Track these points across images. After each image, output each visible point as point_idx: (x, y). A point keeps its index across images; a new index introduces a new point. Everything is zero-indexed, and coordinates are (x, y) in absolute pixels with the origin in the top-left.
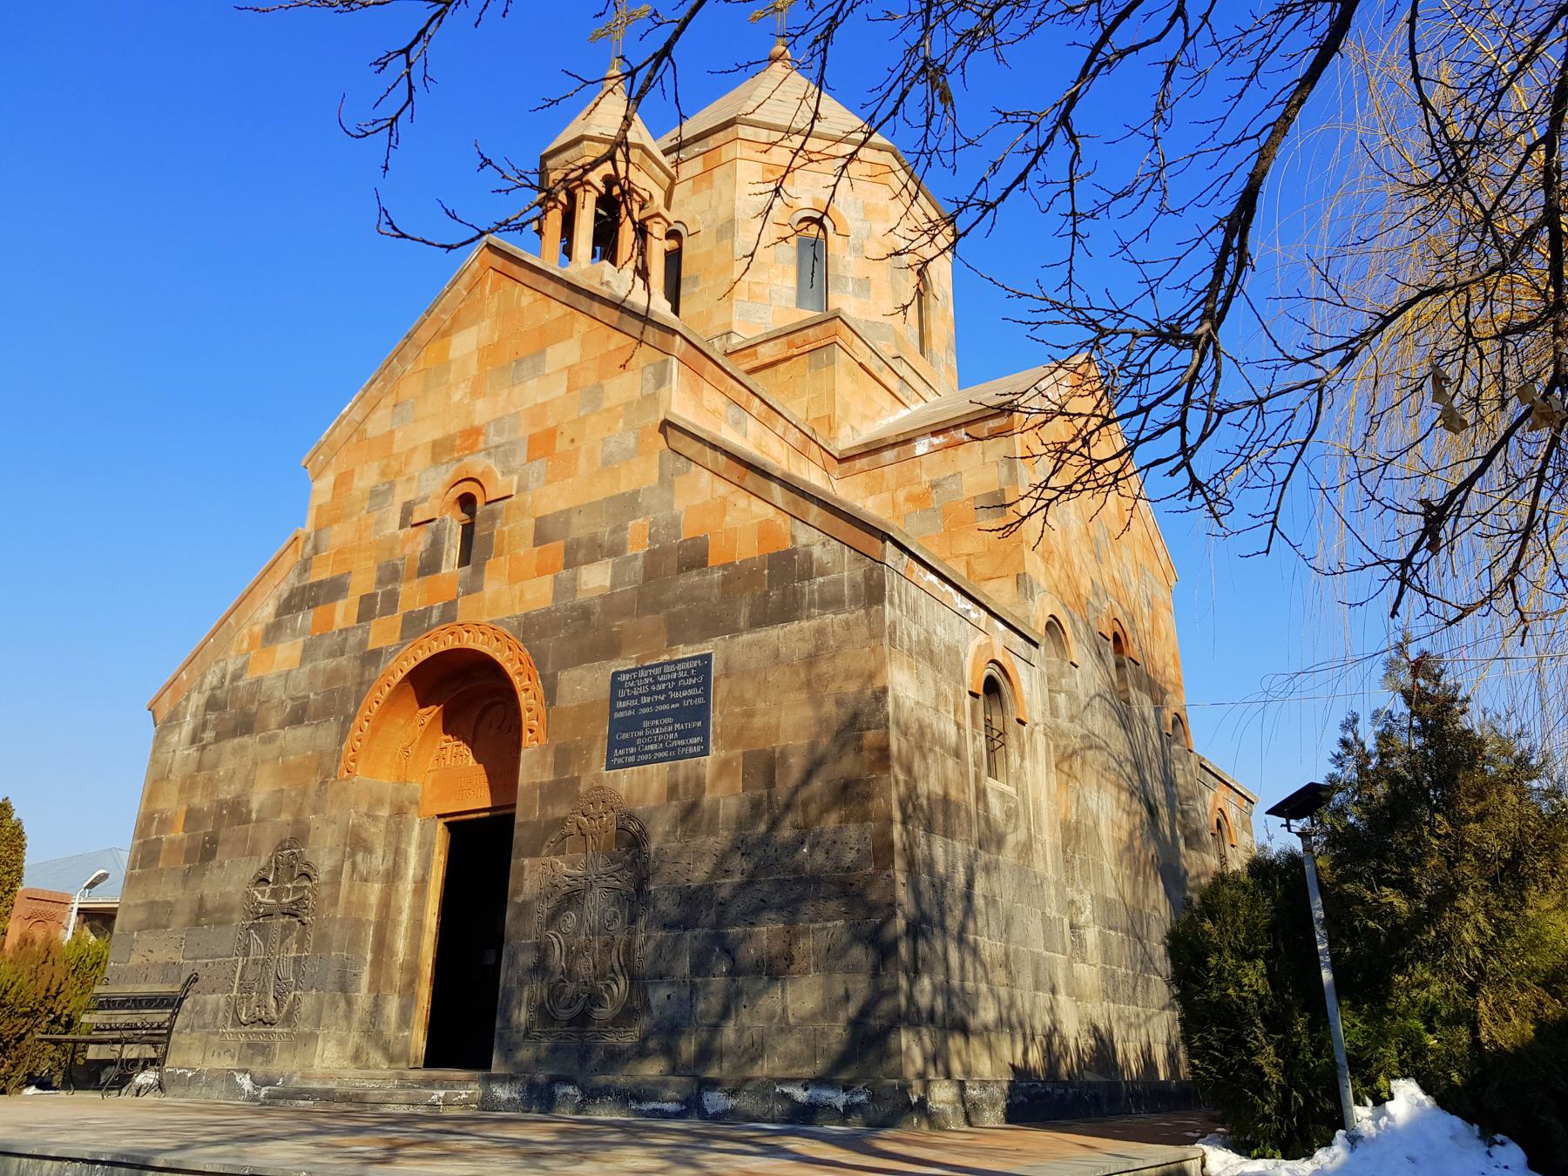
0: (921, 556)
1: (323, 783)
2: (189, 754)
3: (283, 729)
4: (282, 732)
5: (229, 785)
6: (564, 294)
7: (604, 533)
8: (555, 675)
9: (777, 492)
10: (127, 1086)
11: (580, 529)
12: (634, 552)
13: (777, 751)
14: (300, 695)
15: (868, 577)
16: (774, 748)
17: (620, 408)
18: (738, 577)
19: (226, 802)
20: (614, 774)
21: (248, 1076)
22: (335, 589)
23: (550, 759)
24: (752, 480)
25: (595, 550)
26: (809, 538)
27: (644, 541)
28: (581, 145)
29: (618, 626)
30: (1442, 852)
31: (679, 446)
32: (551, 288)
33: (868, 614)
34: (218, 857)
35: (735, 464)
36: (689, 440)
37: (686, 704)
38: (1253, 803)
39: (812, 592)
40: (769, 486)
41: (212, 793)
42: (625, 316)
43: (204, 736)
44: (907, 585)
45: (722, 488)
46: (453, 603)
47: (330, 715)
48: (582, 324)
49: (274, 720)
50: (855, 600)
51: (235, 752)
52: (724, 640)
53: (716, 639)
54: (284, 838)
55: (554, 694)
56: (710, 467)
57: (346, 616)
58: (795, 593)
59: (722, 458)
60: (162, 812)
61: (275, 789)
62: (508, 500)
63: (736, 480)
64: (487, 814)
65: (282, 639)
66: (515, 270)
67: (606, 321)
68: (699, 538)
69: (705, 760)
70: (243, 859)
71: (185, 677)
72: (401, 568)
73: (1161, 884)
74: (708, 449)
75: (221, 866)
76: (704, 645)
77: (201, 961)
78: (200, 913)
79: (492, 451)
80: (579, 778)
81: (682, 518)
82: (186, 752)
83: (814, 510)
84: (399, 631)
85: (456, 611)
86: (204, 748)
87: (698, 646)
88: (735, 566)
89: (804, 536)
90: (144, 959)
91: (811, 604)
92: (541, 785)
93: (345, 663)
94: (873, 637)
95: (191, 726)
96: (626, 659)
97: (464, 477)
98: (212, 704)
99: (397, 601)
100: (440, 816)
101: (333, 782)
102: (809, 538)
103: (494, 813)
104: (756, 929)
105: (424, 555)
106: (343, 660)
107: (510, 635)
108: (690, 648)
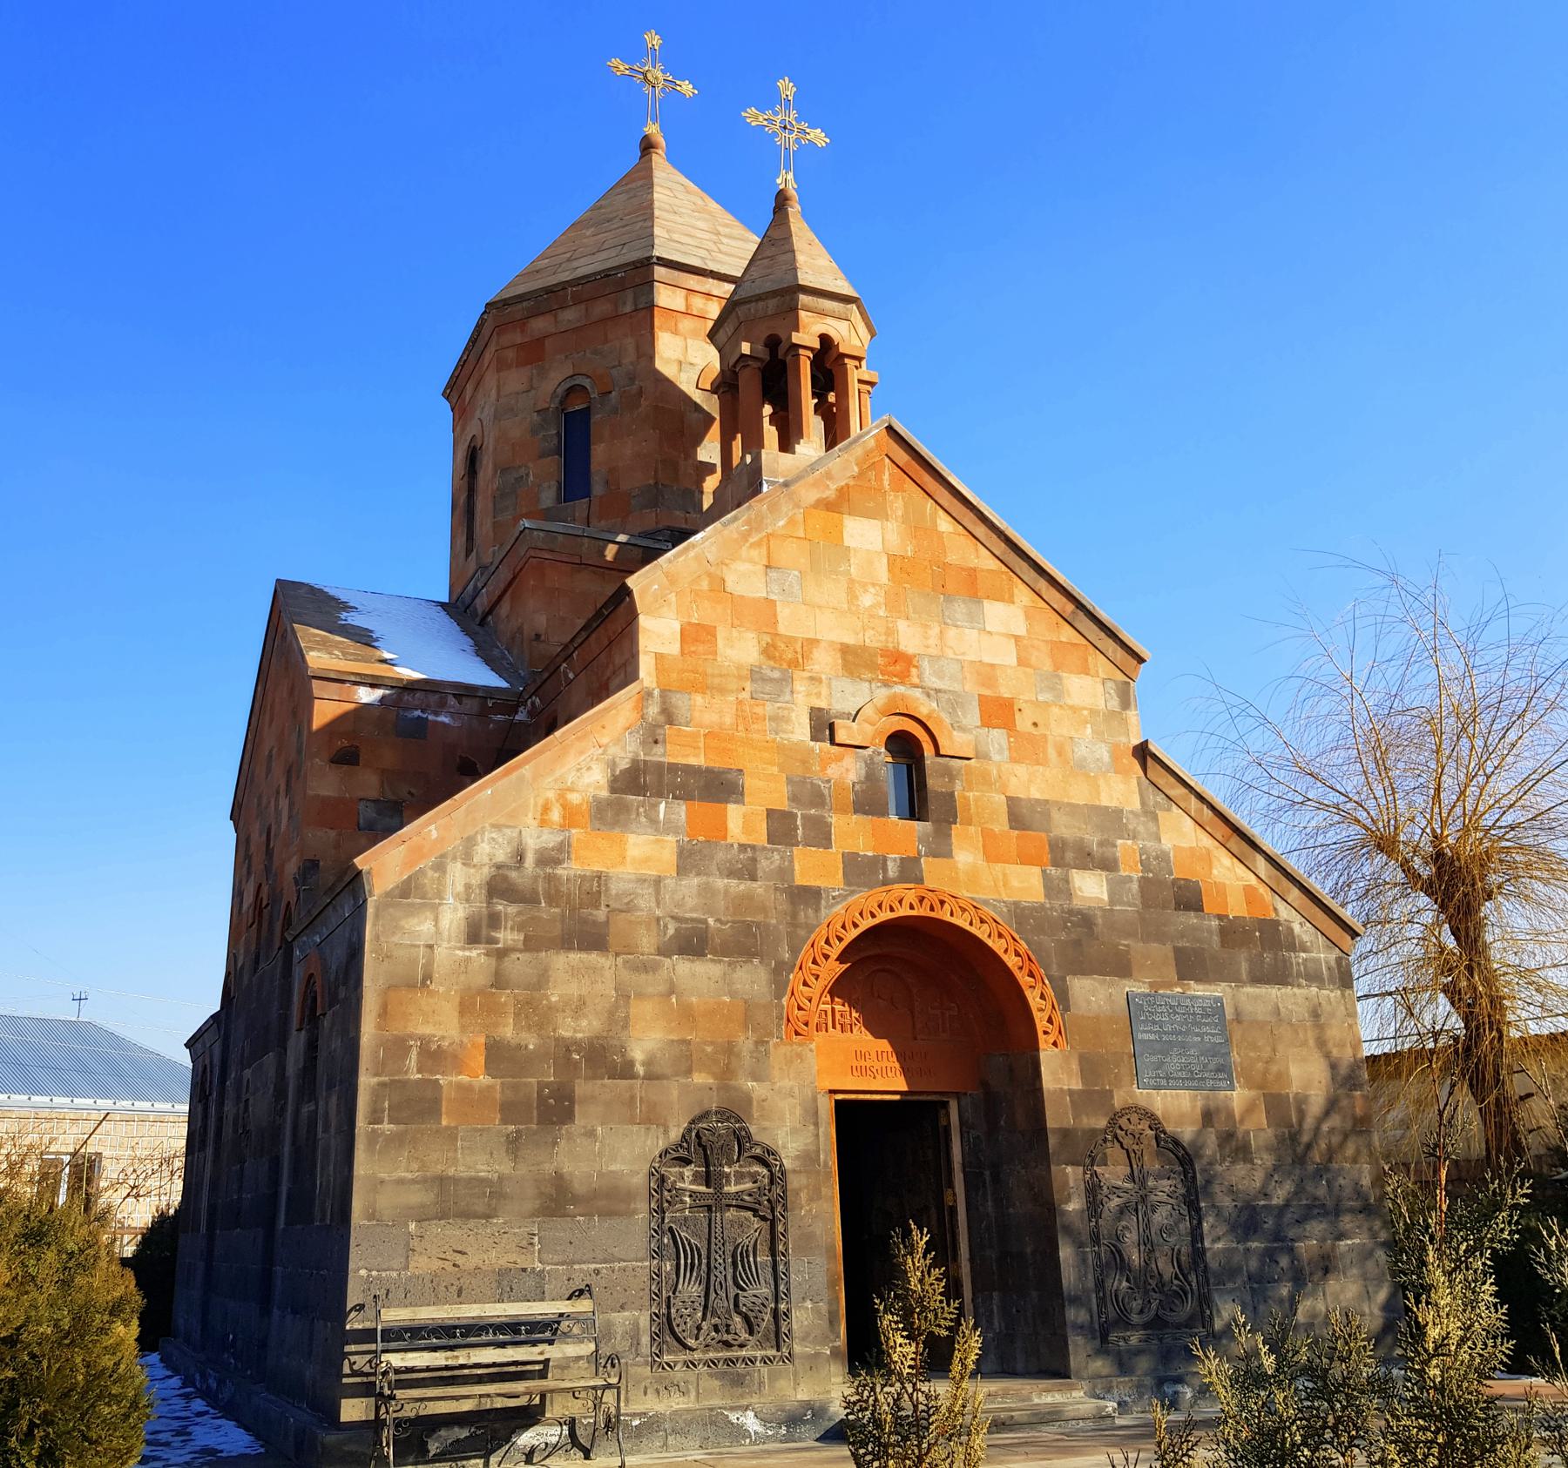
2: (468, 959)
3: (669, 956)
7: (1093, 839)
9: (1261, 864)
10: (501, 1452)
12: (1127, 873)
14: (688, 915)
15: (1339, 960)
17: (1085, 712)
20: (1177, 1094)
21: (750, 1414)
23: (1075, 1066)
24: (1236, 843)
28: (849, 306)
29: (1125, 945)
31: (1161, 782)
32: (981, 530)
33: (1343, 995)
34: (579, 1121)
37: (1207, 1039)
39: (1298, 964)
41: (540, 1026)
42: (1081, 613)
44: (1000, 894)
45: (1207, 841)
47: (754, 955)
48: (1023, 595)
49: (647, 942)
50: (1332, 981)
51: (574, 971)
53: (1223, 984)
54: (706, 1107)
55: (1067, 1000)
56: (1193, 814)
58: (1284, 961)
59: (1207, 812)
63: (1220, 838)
64: (897, 1097)
65: (633, 826)
66: (927, 480)
67: (1055, 607)
68: (1190, 881)
70: (635, 1128)
74: (1193, 798)
75: (591, 1134)
76: (1213, 987)
77: (584, 1266)
79: (932, 692)
80: (1111, 1091)
81: (1171, 855)
82: (460, 953)
83: (1294, 894)
84: (841, 872)
86: (501, 954)
88: (1229, 920)
89: (1285, 913)
91: (1299, 975)
92: (1071, 1092)
93: (760, 891)
95: (461, 914)
96: (1139, 981)
97: (906, 712)
98: (499, 887)
103: (904, 1098)
104: (1296, 1244)
106: (758, 888)
107: (998, 920)
108: (1201, 987)
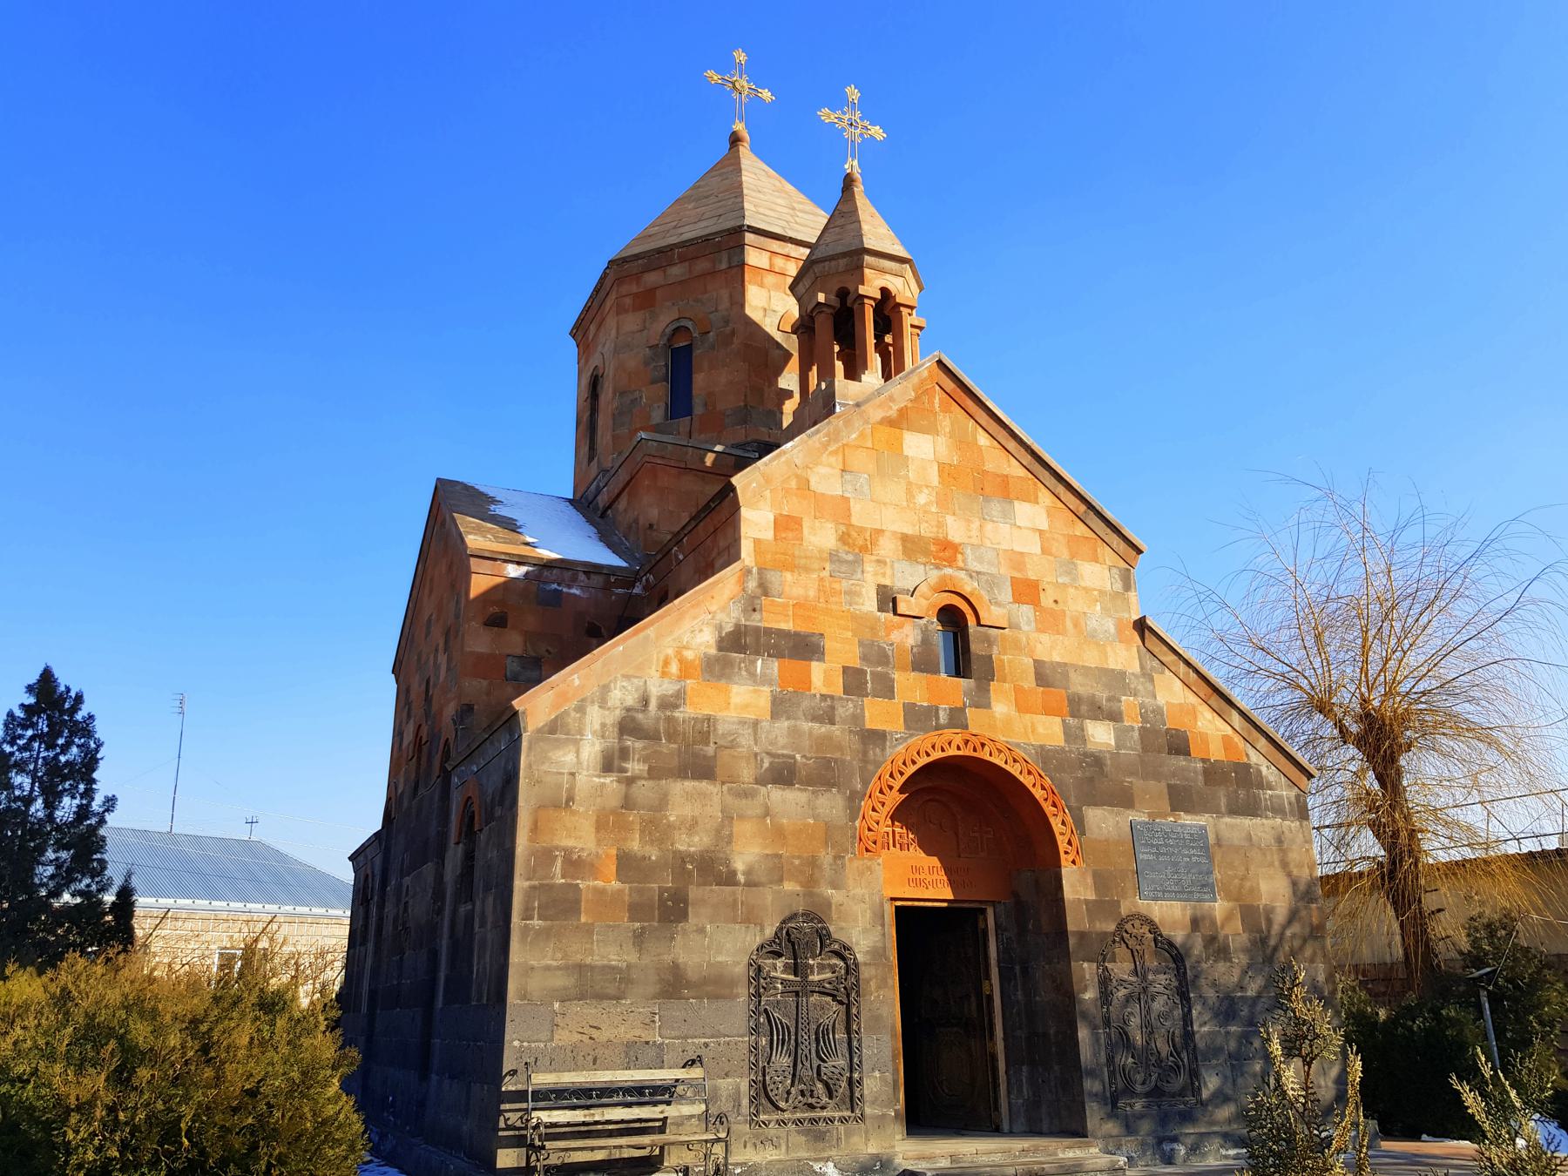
0: (988, 403)
1: (837, 857)
2: (603, 785)
4: (763, 790)
5: (690, 835)
6: (1027, 459)
8: (1080, 809)
9: (1236, 718)
11: (1080, 686)
13: (1261, 907)
16: (1259, 905)
18: (1214, 773)
19: (691, 855)
21: (831, 1164)
22: (804, 647)
23: (1090, 880)
24: (1215, 701)
25: (1100, 712)
26: (1258, 758)
27: (1137, 717)
30: (186, 1099)
32: (1012, 445)
33: (1301, 825)
34: (692, 919)
35: (1205, 685)
36: (1165, 648)
38: (1139, 552)
39: (1265, 799)
40: (1230, 711)
43: (629, 766)
46: (962, 710)
48: (1045, 497)
51: (688, 796)
52: (1212, 817)
54: (794, 910)
57: (828, 681)
59: (1193, 676)
60: (565, 849)
61: (768, 852)
62: (1002, 631)
63: (1203, 697)
64: (945, 905)
67: (1071, 507)
69: (1214, 905)
71: (577, 682)
72: (890, 653)
73: (1083, 1064)
78: (674, 985)
85: (966, 719)
87: (1194, 817)
90: (585, 1038)
91: (1267, 808)
92: (1087, 902)
94: (1306, 842)
98: (628, 726)
99: (893, 687)
100: (893, 899)
101: (851, 859)
102: (1258, 758)
105: (915, 650)
106: (836, 730)
